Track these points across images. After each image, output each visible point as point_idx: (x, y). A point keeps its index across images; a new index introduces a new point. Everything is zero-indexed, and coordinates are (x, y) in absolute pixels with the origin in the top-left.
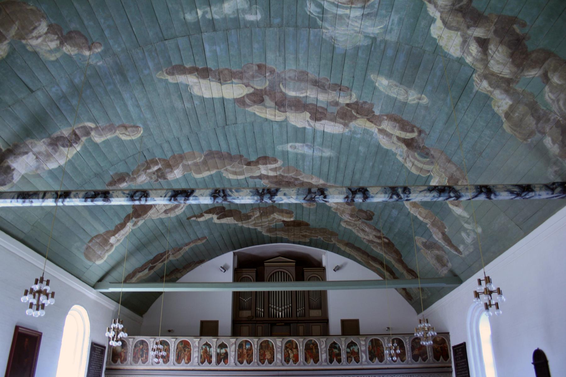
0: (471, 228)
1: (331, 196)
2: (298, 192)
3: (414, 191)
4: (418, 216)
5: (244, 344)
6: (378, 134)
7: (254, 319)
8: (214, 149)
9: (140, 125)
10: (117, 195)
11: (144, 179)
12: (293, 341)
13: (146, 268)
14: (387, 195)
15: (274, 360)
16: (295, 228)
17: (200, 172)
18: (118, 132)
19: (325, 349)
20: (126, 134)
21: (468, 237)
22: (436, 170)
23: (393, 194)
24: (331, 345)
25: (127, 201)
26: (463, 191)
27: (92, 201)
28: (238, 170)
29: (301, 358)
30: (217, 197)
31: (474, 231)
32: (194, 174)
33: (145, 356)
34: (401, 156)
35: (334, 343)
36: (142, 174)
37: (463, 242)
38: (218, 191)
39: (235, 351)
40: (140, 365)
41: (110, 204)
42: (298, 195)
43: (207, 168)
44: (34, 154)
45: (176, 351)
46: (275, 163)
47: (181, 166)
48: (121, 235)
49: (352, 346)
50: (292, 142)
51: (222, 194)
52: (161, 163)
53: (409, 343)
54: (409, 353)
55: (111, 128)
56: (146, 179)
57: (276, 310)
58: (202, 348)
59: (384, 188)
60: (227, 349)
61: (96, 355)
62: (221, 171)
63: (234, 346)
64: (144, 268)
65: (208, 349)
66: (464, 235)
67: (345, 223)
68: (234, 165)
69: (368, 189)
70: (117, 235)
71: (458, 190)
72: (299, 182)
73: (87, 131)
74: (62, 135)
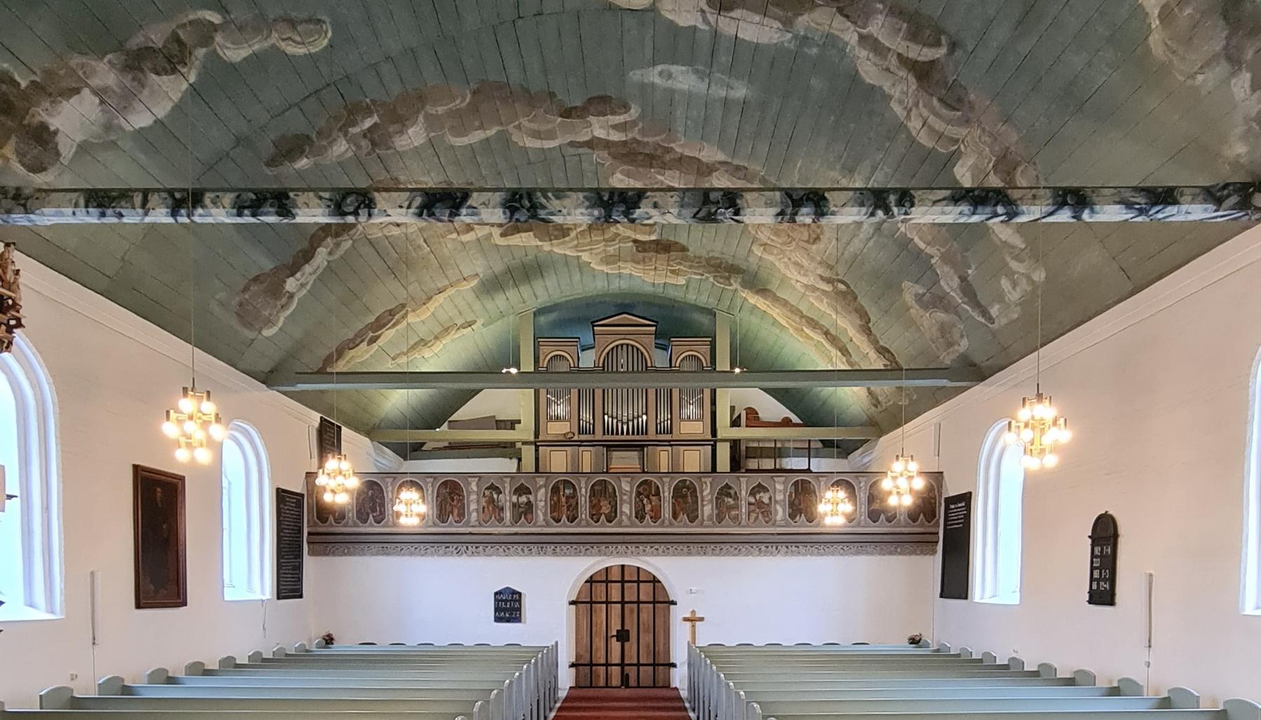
0: (1024, 271)
1: (749, 210)
2: (683, 199)
3: (921, 200)
4: (917, 240)
5: (562, 487)
6: (857, 48)
7: (576, 438)
8: (492, 77)
9: (324, 18)
10: (307, 201)
11: (343, 148)
12: (651, 481)
13: (362, 341)
14: (864, 210)
15: (616, 516)
16: (658, 255)
17: (461, 131)
18: (275, 35)
19: (710, 497)
20: (294, 41)
21: (1014, 288)
22: (973, 138)
23: (877, 207)
24: (722, 489)
25: (329, 215)
26: (1025, 202)
27: (254, 215)
28: (543, 128)
29: (667, 511)
30: (517, 209)
31: (1029, 278)
32: (450, 137)
33: (378, 509)
34: (900, 102)
35: (728, 486)
36: (339, 137)
37: (1000, 298)
38: (517, 196)
39: (546, 501)
40: (371, 525)
41: (293, 221)
42: (682, 206)
43: (477, 124)
44: (95, 92)
45: (437, 500)
46: (625, 113)
47: (421, 118)
48: (306, 275)
49: (759, 492)
50: (664, 63)
51: (527, 203)
52: (377, 111)
53: (866, 489)
54: (863, 506)
55: (262, 24)
56: (347, 149)
57: (613, 418)
58: (484, 494)
59: (861, 194)
60: (530, 496)
61: (288, 510)
62: (507, 130)
63: (543, 490)
64: (359, 340)
65: (495, 496)
66: (1005, 283)
67: (762, 248)
68: (535, 116)
69: (826, 195)
70: (298, 275)
71: (1015, 201)
72: (672, 157)
73: (206, 33)
74: (151, 44)
